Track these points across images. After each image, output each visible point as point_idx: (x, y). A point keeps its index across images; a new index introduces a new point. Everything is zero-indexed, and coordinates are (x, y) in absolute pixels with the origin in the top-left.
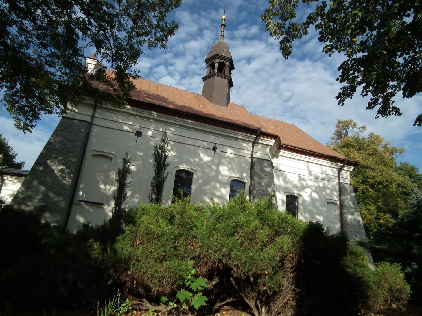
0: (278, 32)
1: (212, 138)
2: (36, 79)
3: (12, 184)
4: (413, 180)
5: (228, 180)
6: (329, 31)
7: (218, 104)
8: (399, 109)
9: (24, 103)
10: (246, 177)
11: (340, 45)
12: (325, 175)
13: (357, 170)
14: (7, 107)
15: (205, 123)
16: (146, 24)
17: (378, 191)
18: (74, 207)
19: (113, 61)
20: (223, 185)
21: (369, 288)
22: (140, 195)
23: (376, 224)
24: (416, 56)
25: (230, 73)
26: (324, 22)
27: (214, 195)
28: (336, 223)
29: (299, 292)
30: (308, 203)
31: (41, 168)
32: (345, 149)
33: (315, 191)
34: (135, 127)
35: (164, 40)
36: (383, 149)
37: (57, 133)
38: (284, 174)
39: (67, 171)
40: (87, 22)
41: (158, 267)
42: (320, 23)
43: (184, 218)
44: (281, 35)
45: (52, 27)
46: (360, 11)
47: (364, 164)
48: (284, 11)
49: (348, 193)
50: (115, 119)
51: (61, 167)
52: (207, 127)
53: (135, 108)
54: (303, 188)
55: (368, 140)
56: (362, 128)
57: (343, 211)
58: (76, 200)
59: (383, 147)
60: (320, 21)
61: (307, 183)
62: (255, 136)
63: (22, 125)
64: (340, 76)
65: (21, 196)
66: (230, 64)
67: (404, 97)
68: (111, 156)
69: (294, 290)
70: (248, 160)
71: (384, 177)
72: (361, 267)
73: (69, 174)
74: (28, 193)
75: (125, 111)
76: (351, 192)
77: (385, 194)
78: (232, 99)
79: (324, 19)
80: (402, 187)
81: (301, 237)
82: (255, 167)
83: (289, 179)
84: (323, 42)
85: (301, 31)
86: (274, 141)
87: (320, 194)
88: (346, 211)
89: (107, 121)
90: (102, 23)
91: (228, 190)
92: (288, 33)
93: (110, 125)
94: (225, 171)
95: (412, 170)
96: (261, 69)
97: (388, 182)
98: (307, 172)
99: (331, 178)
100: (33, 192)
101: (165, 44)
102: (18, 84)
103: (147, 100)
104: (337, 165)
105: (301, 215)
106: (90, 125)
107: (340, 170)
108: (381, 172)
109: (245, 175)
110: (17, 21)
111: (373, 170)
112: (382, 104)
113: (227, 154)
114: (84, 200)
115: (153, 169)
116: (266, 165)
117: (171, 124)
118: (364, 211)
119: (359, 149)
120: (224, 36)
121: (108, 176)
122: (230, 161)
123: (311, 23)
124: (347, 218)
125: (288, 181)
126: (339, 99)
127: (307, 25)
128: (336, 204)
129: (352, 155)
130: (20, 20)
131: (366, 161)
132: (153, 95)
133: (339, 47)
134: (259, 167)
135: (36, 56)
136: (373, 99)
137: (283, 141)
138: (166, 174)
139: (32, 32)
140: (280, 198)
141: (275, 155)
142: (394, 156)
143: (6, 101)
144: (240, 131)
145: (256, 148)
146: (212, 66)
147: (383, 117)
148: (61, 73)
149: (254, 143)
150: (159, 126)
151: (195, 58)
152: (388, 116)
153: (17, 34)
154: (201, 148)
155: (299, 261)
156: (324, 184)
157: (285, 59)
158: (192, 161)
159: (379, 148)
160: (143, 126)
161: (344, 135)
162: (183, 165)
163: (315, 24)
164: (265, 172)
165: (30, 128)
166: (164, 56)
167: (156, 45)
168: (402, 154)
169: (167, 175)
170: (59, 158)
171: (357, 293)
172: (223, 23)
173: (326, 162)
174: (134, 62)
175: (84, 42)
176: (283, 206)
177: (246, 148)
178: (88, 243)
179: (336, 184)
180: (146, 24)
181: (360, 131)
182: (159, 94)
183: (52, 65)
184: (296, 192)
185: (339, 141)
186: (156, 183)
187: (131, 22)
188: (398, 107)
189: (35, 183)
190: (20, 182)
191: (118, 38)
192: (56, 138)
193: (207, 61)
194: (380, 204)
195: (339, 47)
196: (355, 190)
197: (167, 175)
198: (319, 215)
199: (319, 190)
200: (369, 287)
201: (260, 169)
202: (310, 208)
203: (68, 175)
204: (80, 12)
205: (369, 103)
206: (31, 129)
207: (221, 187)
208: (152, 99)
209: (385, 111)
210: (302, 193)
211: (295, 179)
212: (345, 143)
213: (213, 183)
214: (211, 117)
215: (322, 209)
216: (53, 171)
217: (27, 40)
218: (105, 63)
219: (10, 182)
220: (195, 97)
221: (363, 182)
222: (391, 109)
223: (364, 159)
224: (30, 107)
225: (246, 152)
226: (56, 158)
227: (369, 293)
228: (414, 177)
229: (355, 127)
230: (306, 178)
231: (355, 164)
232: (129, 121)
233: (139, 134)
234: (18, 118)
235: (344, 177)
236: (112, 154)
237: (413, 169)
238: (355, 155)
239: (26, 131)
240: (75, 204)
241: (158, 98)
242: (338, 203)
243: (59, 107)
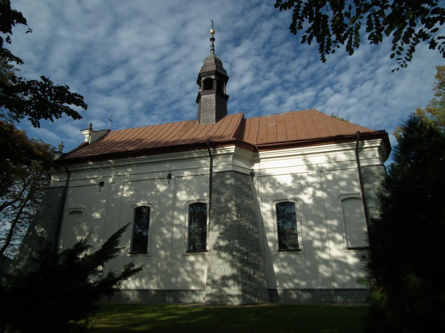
1: (168, 166)
12: (335, 164)
20: (181, 211)
27: (173, 225)
33: (322, 189)
34: (98, 178)
38: (272, 178)
50: (84, 177)
52: (159, 157)
53: (96, 163)
54: (301, 189)
61: (306, 181)
68: (82, 210)
75: (89, 167)
83: (279, 183)
86: (234, 147)
87: (329, 190)
98: (305, 167)
99: (347, 165)
106: (65, 189)
107: (358, 150)
113: (184, 178)
116: (228, 177)
125: (278, 185)
140: (267, 209)
150: (118, 171)
151: (361, 66)
158: (149, 195)
160: (105, 176)
162: (140, 202)
166: (327, 78)
173: (333, 147)
198: (331, 219)
202: (314, 212)
207: (179, 214)
211: (288, 181)
215: (335, 210)
230: (305, 175)
233: (102, 184)
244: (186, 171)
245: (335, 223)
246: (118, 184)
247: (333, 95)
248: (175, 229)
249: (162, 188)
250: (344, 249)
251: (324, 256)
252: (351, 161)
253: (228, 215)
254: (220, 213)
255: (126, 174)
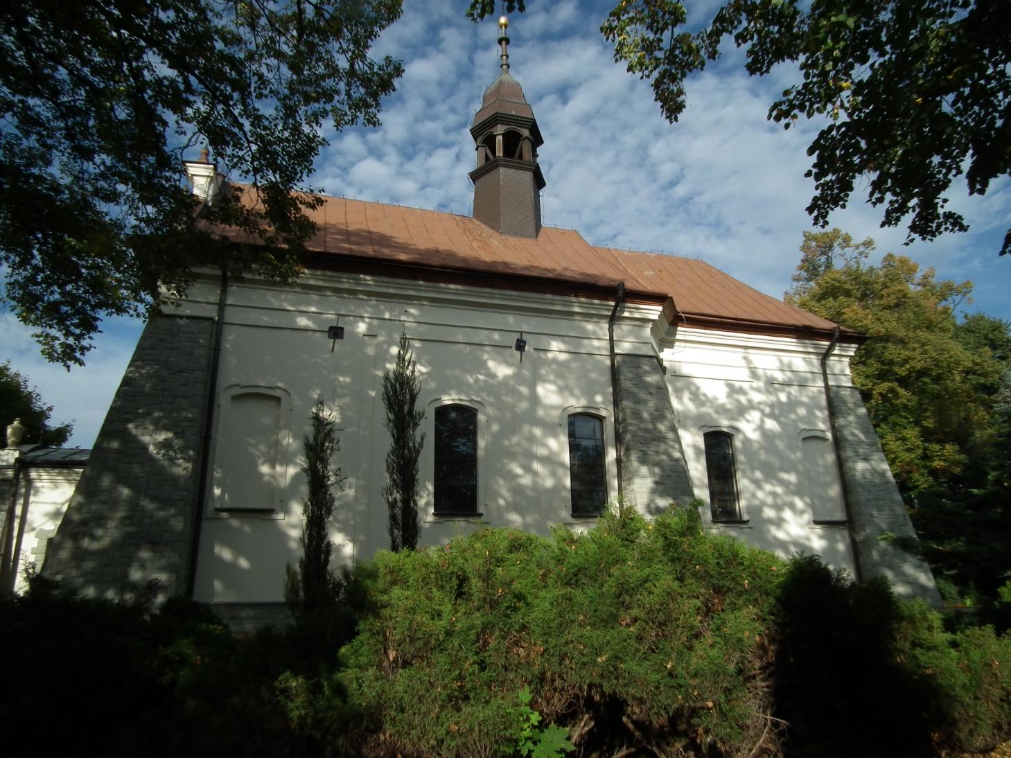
0: (647, 61)
1: (511, 320)
2: (79, 240)
3: (52, 489)
4: (999, 353)
5: (561, 417)
6: (771, 47)
7: (515, 234)
8: (960, 217)
9: (57, 296)
10: (603, 403)
11: (809, 100)
12: (789, 374)
13: (865, 349)
14: (17, 311)
15: (491, 286)
16: (321, 69)
17: (921, 392)
18: (206, 526)
19: (256, 171)
20: (550, 428)
21: (956, 701)
22: (358, 478)
23: (923, 471)
24: (988, 87)
25: (535, 155)
26: (755, 24)
27: (532, 456)
28: (828, 485)
29: (788, 727)
30: (756, 446)
31: (115, 445)
32: (830, 302)
33: (772, 416)
35: (371, 106)
36: (919, 288)
37: (140, 357)
39: (178, 443)
40: (182, 87)
41: (451, 722)
42: (746, 29)
43: (493, 587)
44: (655, 68)
45: (100, 107)
46: (849, 14)
47: (880, 332)
48: (656, 9)
49: (850, 409)
50: (276, 304)
51: (162, 437)
53: (319, 272)
54: (741, 411)
55: (881, 273)
56: (864, 244)
57: (844, 455)
58: (210, 508)
59: (919, 285)
60: (745, 24)
61: (749, 397)
62: (613, 303)
63: (59, 351)
64: (815, 166)
65: (76, 517)
66: (531, 133)
67: (971, 193)
68: (278, 393)
69: (775, 725)
70: (601, 362)
71: (930, 357)
72: (929, 649)
73: (184, 449)
74: (94, 507)
76: (857, 406)
77: (937, 397)
78: (546, 222)
79: (756, 20)
80: (974, 374)
81: (778, 599)
82: (622, 378)
83: (705, 395)
84: (758, 74)
85: (702, 52)
86: (661, 308)
87: (783, 419)
88: (849, 453)
89: (258, 312)
90: (217, 85)
91: (564, 439)
92: (671, 58)
93: (266, 319)
94: (549, 394)
95: (995, 330)
96: (598, 113)
97: (942, 367)
99: (806, 379)
100: (104, 503)
101: (375, 115)
102: (35, 252)
103: (345, 247)
104: (816, 346)
105: (745, 476)
106: (217, 327)
107: (825, 357)
108: (923, 345)
109: (599, 398)
110: (13, 102)
111: (903, 342)
112: (917, 210)
113: (550, 355)
114: (226, 506)
115: (385, 429)
116: (647, 368)
117: (409, 298)
118: (893, 445)
119: (864, 297)
120: (508, 66)
121: (277, 443)
122: (561, 370)
123: (725, 30)
124: (855, 470)
125: (703, 398)
126: (816, 213)
127: (715, 35)
128: (824, 439)
129: (848, 314)
130: (21, 97)
131: (882, 323)
132: (357, 234)
133: (807, 104)
134: (630, 375)
135: (70, 179)
136: (897, 201)
137: (681, 306)
138: (418, 439)
139: (52, 123)
140: (691, 440)
141: (667, 341)
142: (949, 303)
143: (14, 298)
144: (576, 296)
145: (619, 331)
146: (489, 142)
147: (924, 239)
148: (136, 219)
149: (613, 319)
150: (382, 307)
152: (935, 236)
153: (17, 132)
154: (487, 348)
155: (780, 655)
156: (789, 394)
157: (671, 123)
158: (471, 381)
159: (911, 287)
160: (343, 313)
161: (823, 268)
162: (450, 395)
163: (735, 32)
164: (646, 386)
165: (78, 355)
167: (353, 120)
168: (968, 295)
169: (422, 439)
170: (156, 414)
171: (925, 715)
172: (503, 36)
173: (790, 343)
174: (306, 166)
175: (181, 133)
176: (697, 460)
177: (594, 333)
178: (277, 684)
179: (820, 392)
180: (321, 69)
181: (861, 253)
182: (373, 229)
183: (112, 197)
184: (724, 423)
185: (812, 284)
186: (399, 462)
187: (286, 71)
188: (959, 213)
189: (106, 481)
190: (69, 481)
191: (262, 116)
192: (142, 368)
193: (476, 133)
194: (929, 423)
195: (807, 104)
196: (866, 396)
197: (422, 439)
198: (788, 471)
199: (778, 411)
200: (954, 699)
201: (637, 381)
202: (763, 456)
203: (182, 452)
204: (162, 63)
205: (887, 211)
206: (81, 357)
207: (546, 435)
208: (357, 244)
209: (924, 227)
210: (742, 425)
211: (716, 392)
212: (827, 288)
213: (526, 428)
214: (501, 269)
215: (792, 456)
216: (144, 447)
217: (44, 145)
218: (235, 178)
219: (47, 484)
220: (458, 225)
221: (882, 376)
222: (942, 220)
223: (878, 319)
224: (72, 304)
225: (596, 343)
226: (148, 414)
227: (956, 714)
228: (1002, 345)
229: (848, 246)
230: (746, 386)
231: (858, 338)
232: (309, 304)
233: (336, 332)
234: (47, 335)
235: (837, 371)
236: (279, 388)
237: (996, 327)
238: (856, 313)
239: (69, 363)
240: (208, 519)
241: (371, 239)
242: (829, 435)
243: (142, 301)
244: (554, 340)
245: (792, 478)
246: (384, 342)
247: (365, 158)
248: (537, 466)
249: (503, 371)
250: (809, 523)
251: (781, 535)
252: (812, 373)
253: (662, 447)
254: (646, 442)
255: (403, 318)
